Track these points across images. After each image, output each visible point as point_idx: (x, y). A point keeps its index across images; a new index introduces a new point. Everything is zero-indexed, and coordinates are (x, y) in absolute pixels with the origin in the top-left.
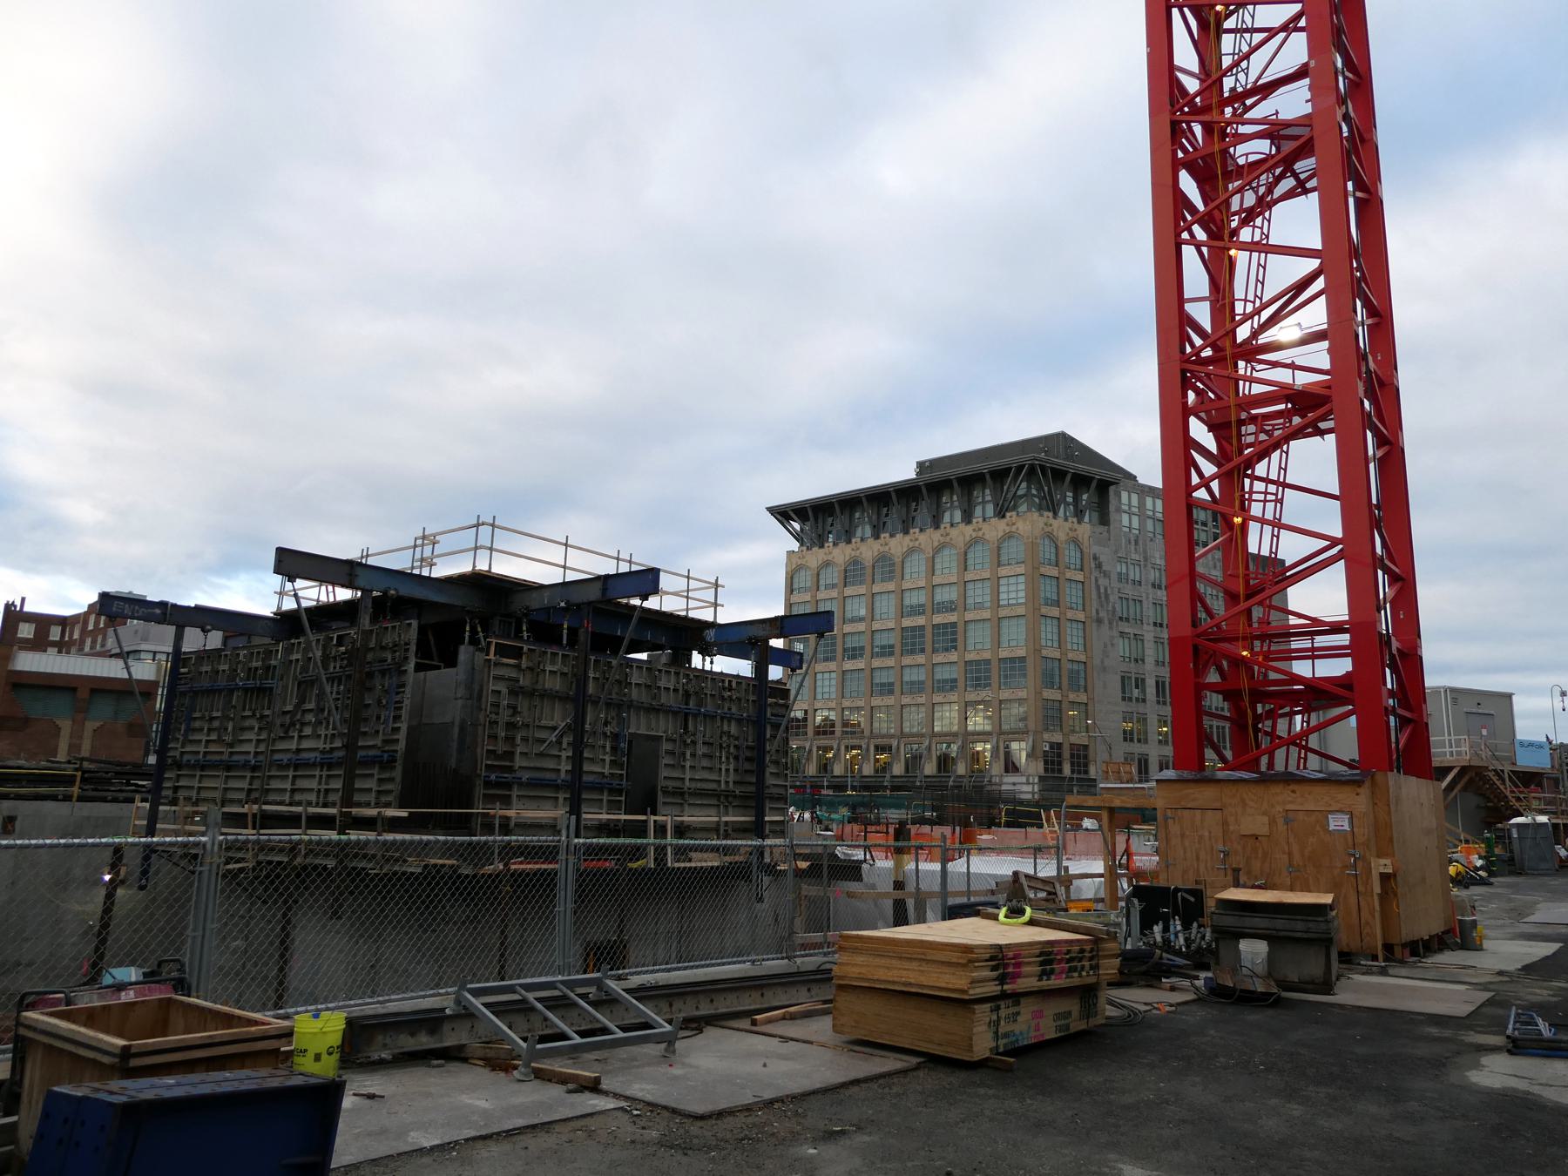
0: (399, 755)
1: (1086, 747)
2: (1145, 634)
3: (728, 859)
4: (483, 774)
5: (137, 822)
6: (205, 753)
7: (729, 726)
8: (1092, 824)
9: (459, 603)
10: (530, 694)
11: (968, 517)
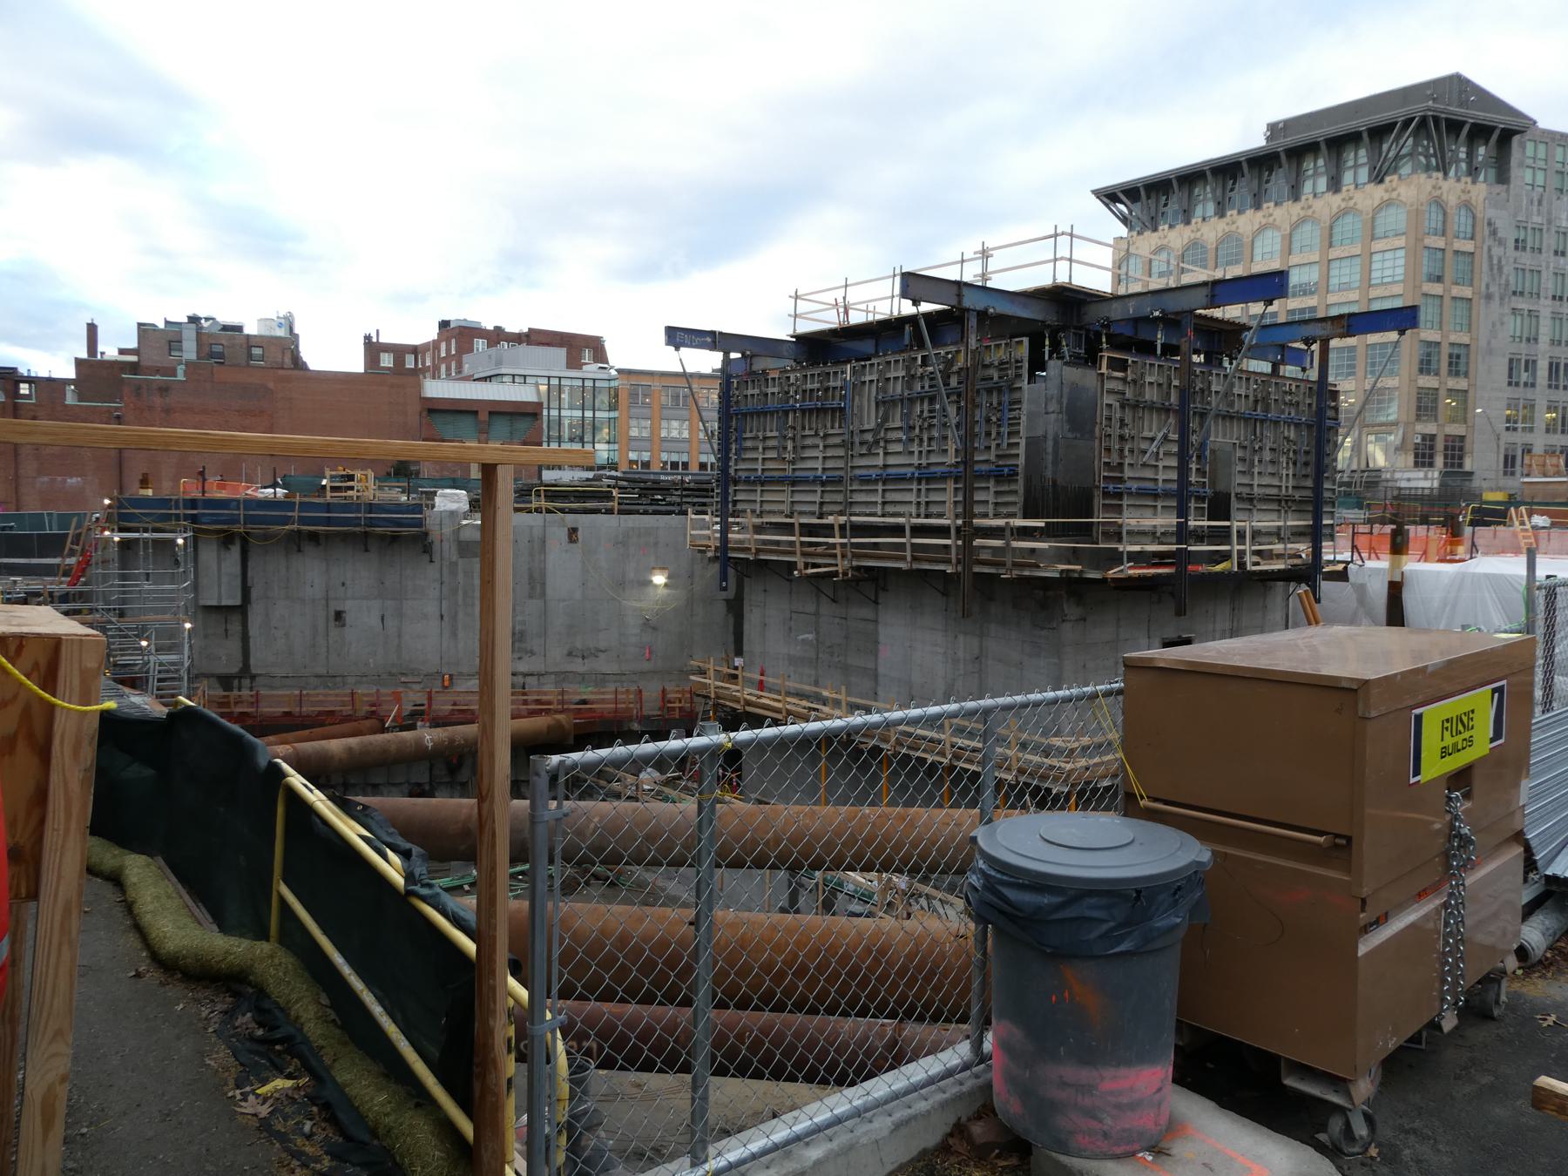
0: (1020, 470)
1: (1462, 438)
2: (1541, 309)
3: (1291, 562)
4: (1102, 485)
5: (693, 532)
6: (763, 470)
7: (1289, 431)
8: (1544, 520)
9: (1039, 317)
10: (1135, 406)
11: (1335, 185)
